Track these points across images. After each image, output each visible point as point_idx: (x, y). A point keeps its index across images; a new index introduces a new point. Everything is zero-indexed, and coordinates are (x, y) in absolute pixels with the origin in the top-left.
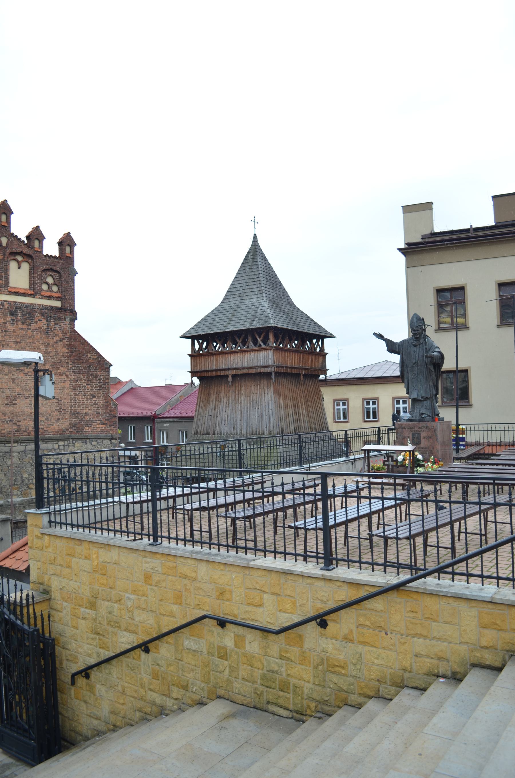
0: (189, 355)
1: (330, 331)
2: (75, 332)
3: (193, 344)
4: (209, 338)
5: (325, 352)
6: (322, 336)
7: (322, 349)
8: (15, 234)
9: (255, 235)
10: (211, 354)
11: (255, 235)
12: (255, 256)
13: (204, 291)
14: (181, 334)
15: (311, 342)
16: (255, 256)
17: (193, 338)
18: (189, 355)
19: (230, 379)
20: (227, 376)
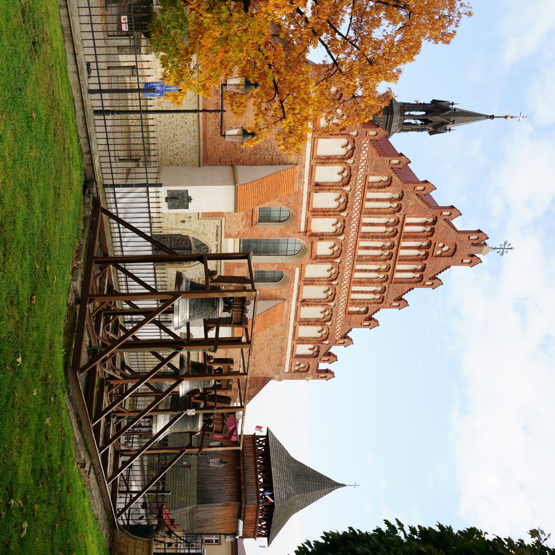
0: (255, 434)
1: (273, 542)
2: (268, 381)
3: (262, 437)
4: (266, 455)
5: (257, 538)
6: (269, 535)
7: (261, 536)
8: (420, 132)
9: (345, 485)
10: (256, 454)
11: (345, 485)
12: (334, 485)
13: (302, 446)
14: (270, 428)
15: (264, 519)
16: (334, 485)
17: (267, 437)
18: (255, 434)
19: (238, 468)
20: (239, 465)
